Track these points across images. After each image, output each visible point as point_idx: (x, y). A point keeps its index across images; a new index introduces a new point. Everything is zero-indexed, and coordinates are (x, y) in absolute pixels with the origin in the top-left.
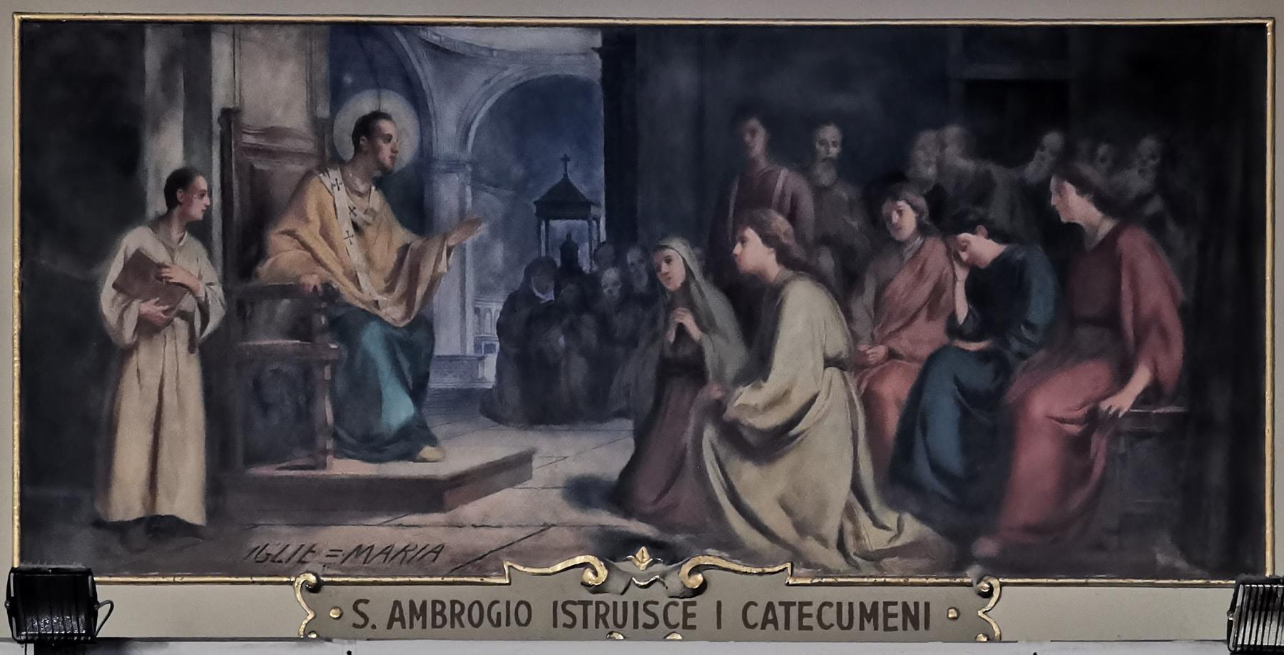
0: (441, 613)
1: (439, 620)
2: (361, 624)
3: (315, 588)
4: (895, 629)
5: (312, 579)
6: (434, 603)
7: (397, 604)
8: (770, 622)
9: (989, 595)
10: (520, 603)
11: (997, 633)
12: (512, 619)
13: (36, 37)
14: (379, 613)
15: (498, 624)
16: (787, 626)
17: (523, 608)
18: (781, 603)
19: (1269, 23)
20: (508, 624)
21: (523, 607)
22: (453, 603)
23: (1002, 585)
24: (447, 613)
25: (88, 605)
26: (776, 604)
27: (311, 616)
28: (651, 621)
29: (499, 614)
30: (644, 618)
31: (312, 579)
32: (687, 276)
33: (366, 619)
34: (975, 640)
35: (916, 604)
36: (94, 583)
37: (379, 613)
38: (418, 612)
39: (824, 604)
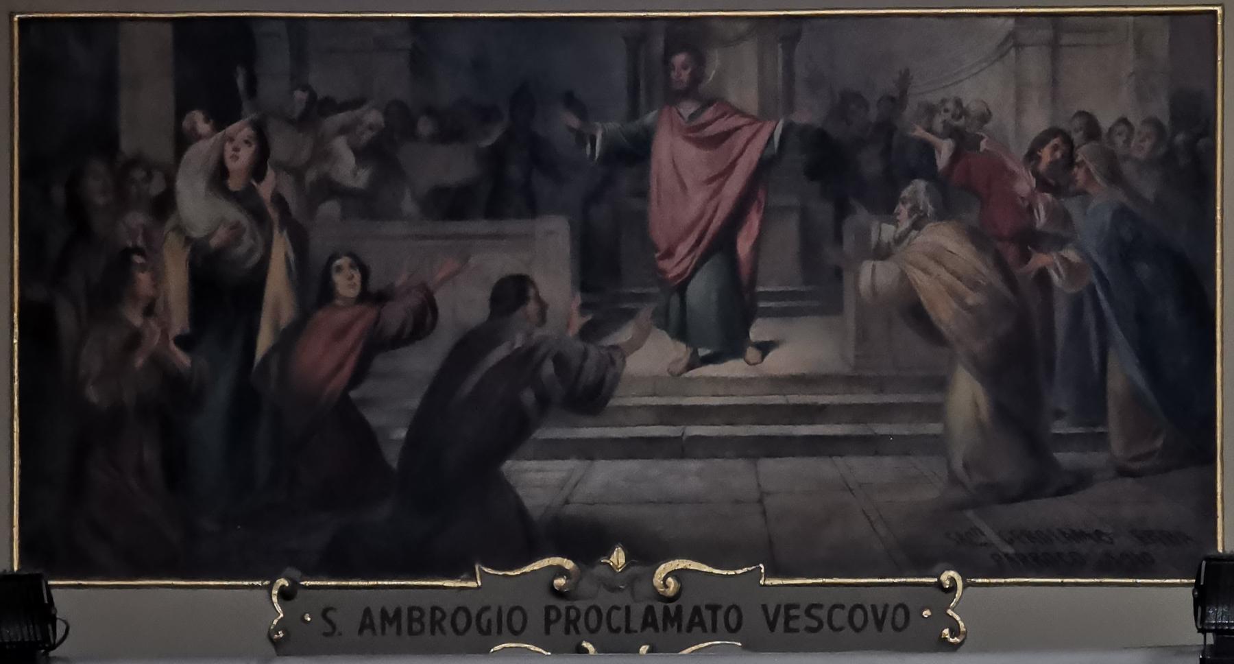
0: (420, 620)
2: (329, 635)
4: (796, 631)
6: (411, 609)
7: (367, 612)
10: (459, 609)
12: (675, 621)
14: (347, 621)
15: (488, 632)
16: (714, 629)
17: (901, 612)
18: (708, 607)
22: (434, 609)
24: (427, 619)
26: (703, 609)
28: (815, 624)
29: (489, 621)
30: (804, 622)
32: (732, 107)
33: (334, 628)
36: (49, 587)
37: (347, 621)
38: (391, 618)
39: (835, 606)
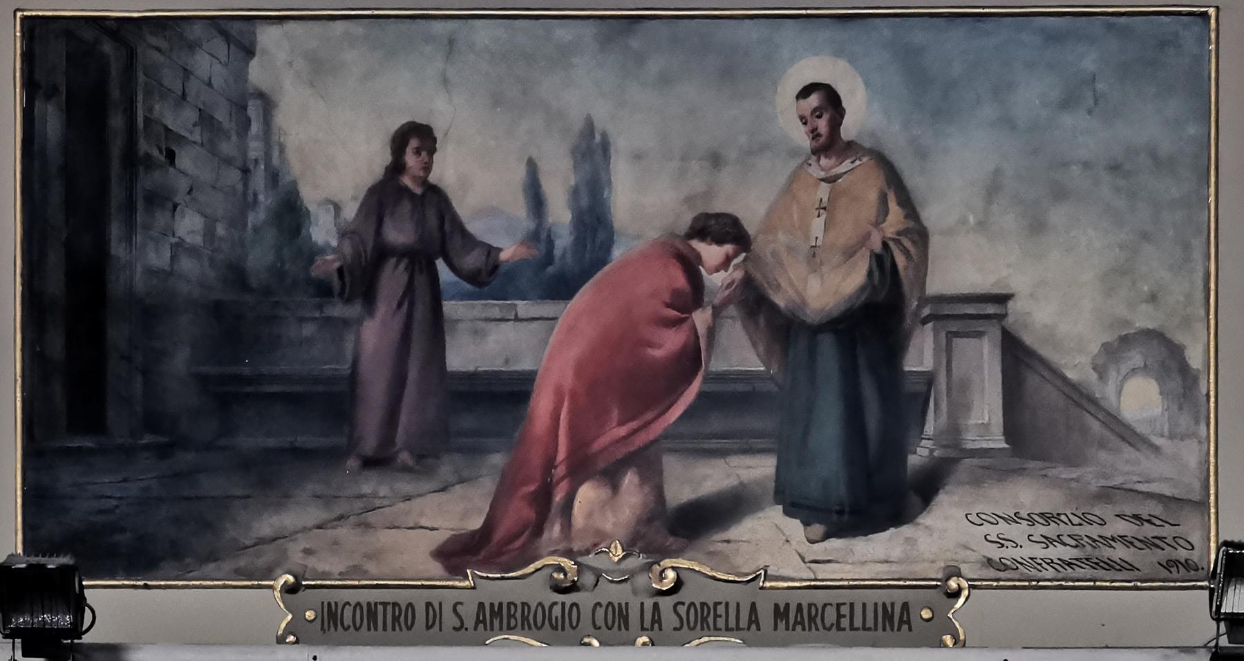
0: (514, 616)
1: (513, 623)
3: (290, 590)
5: (291, 579)
8: (905, 623)
9: (956, 594)
11: (962, 637)
13: (35, 30)
19: (1212, 11)
20: (563, 629)
21: (575, 609)
23: (971, 587)
24: (518, 615)
25: (78, 604)
27: (290, 617)
31: (291, 579)
34: (942, 645)
35: (336, 604)
39: (825, 605)
